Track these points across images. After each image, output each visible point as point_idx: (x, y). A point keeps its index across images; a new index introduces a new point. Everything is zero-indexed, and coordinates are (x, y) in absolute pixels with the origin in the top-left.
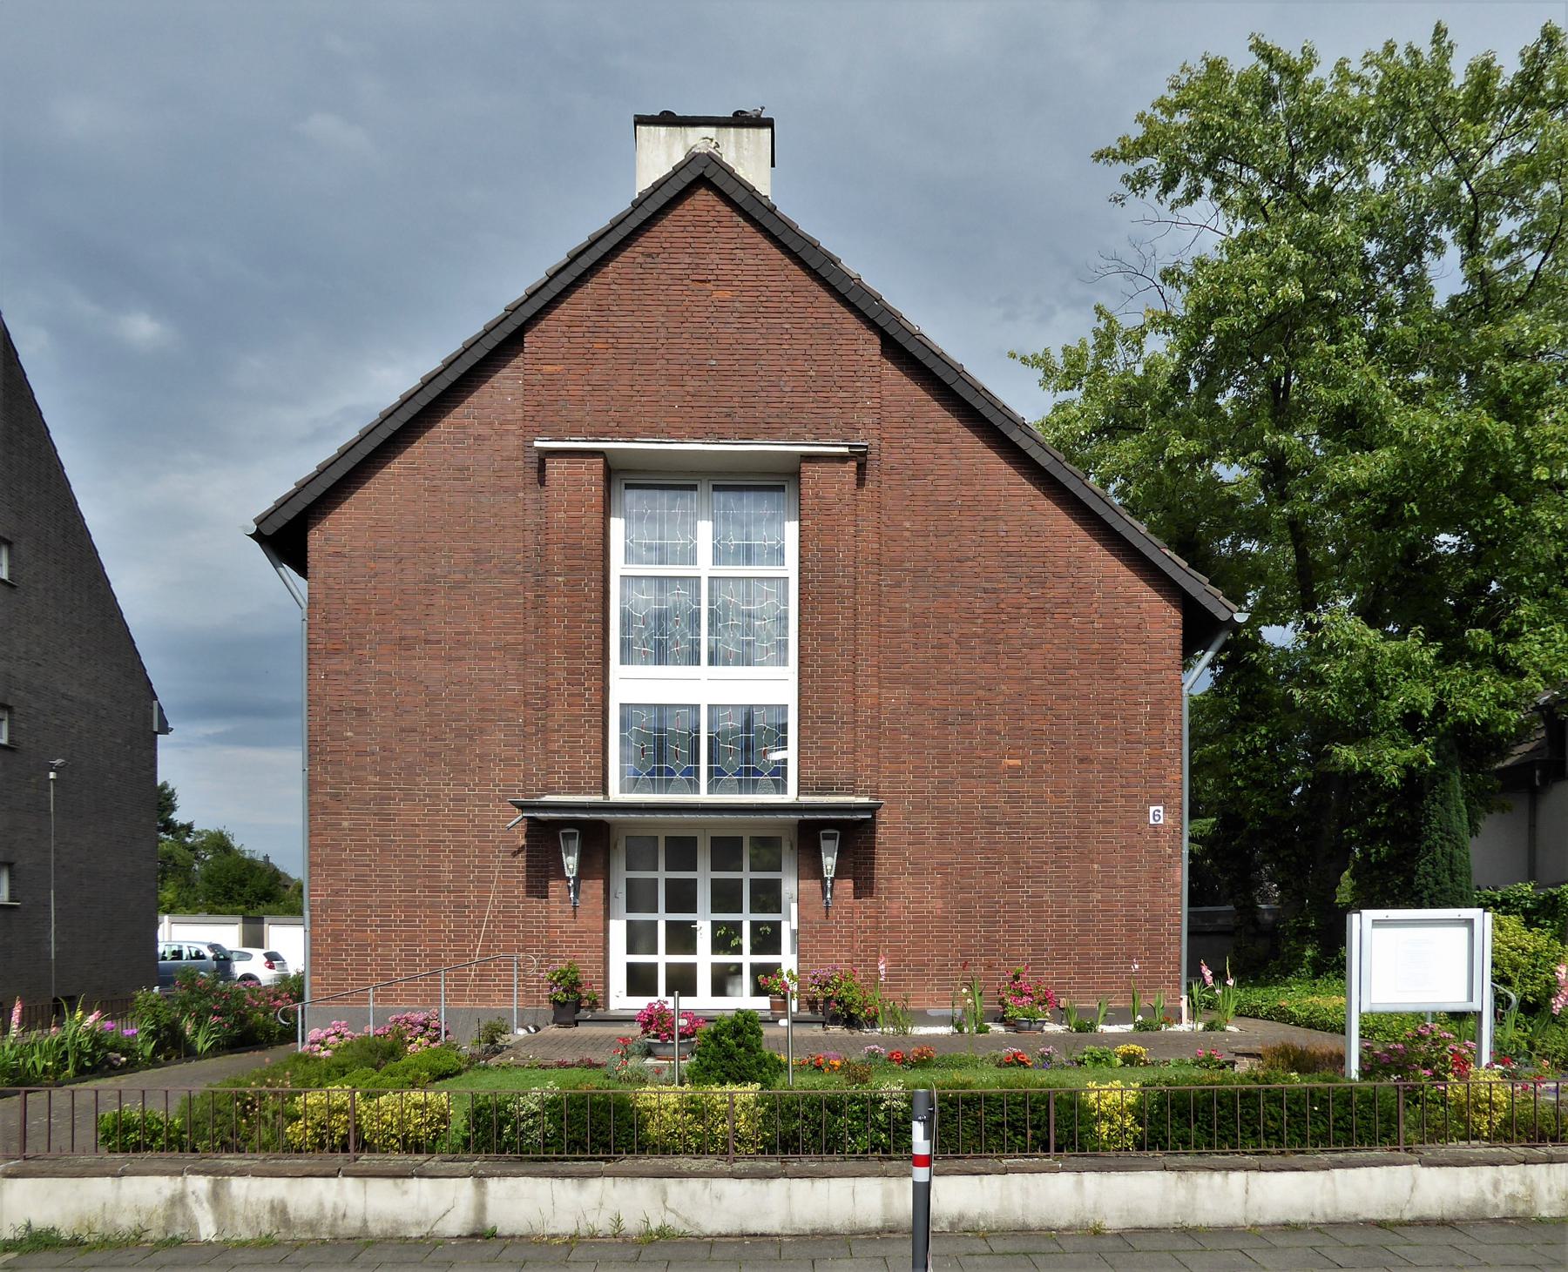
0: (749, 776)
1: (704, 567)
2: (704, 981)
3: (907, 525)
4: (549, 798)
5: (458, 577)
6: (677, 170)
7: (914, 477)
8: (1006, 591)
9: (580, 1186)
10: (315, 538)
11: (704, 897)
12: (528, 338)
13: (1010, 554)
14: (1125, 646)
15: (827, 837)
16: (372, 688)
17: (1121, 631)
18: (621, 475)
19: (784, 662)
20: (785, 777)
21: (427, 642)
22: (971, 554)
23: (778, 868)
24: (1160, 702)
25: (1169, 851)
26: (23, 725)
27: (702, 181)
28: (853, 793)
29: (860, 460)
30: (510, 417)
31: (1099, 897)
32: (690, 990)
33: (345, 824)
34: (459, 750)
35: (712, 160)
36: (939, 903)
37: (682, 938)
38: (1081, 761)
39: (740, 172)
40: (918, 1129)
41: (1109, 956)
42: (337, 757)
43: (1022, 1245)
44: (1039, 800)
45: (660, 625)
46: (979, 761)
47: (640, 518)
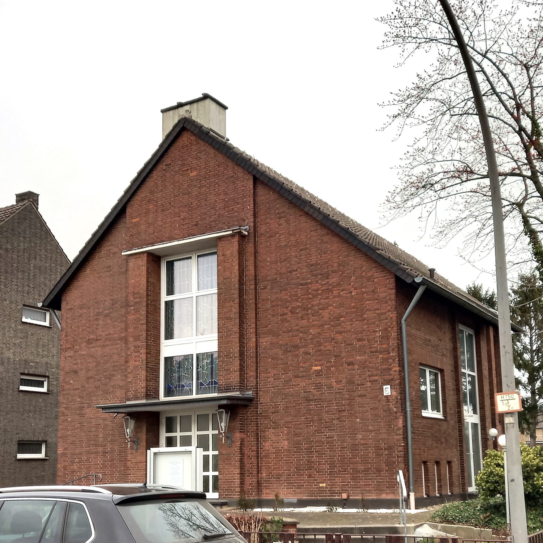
4: (128, 403)
8: (310, 283)
12: (129, 211)
13: (312, 265)
17: (365, 295)
22: (295, 268)
23: (190, 430)
24: (386, 329)
26: (55, 383)
33: (69, 419)
34: (106, 384)
38: (348, 365)
41: (366, 470)
44: (330, 387)
46: (301, 369)
47: (409, 275)
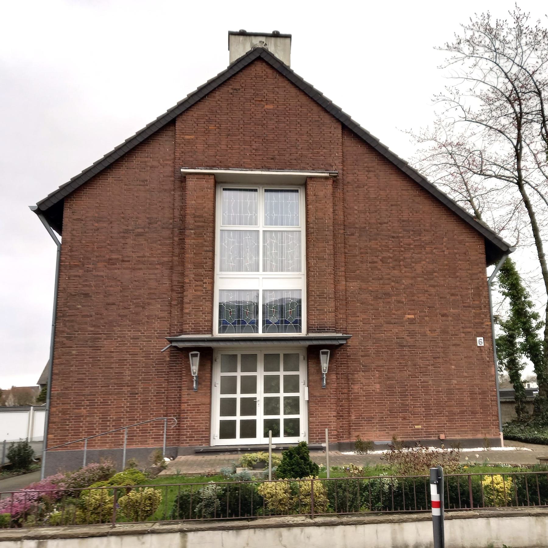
0: (283, 324)
1: (261, 227)
2: (260, 429)
3: (356, 208)
5: (140, 230)
6: (248, 54)
7: (358, 187)
8: (402, 237)
9: (237, 534)
10: (67, 213)
11: (260, 385)
13: (403, 221)
14: (460, 262)
15: (324, 353)
16: (93, 283)
17: (457, 256)
18: (219, 182)
19: (300, 270)
20: (300, 324)
21: (123, 261)
22: (386, 221)
25: (488, 359)
27: (259, 59)
28: (336, 331)
29: (335, 179)
30: (168, 158)
31: (455, 382)
32: (253, 435)
34: (137, 314)
35: (264, 51)
36: (378, 386)
37: (249, 407)
39: (276, 56)
40: (433, 488)
41: (462, 412)
42: (72, 318)
43: (341, 259)
45: (240, 252)
46: (394, 316)
